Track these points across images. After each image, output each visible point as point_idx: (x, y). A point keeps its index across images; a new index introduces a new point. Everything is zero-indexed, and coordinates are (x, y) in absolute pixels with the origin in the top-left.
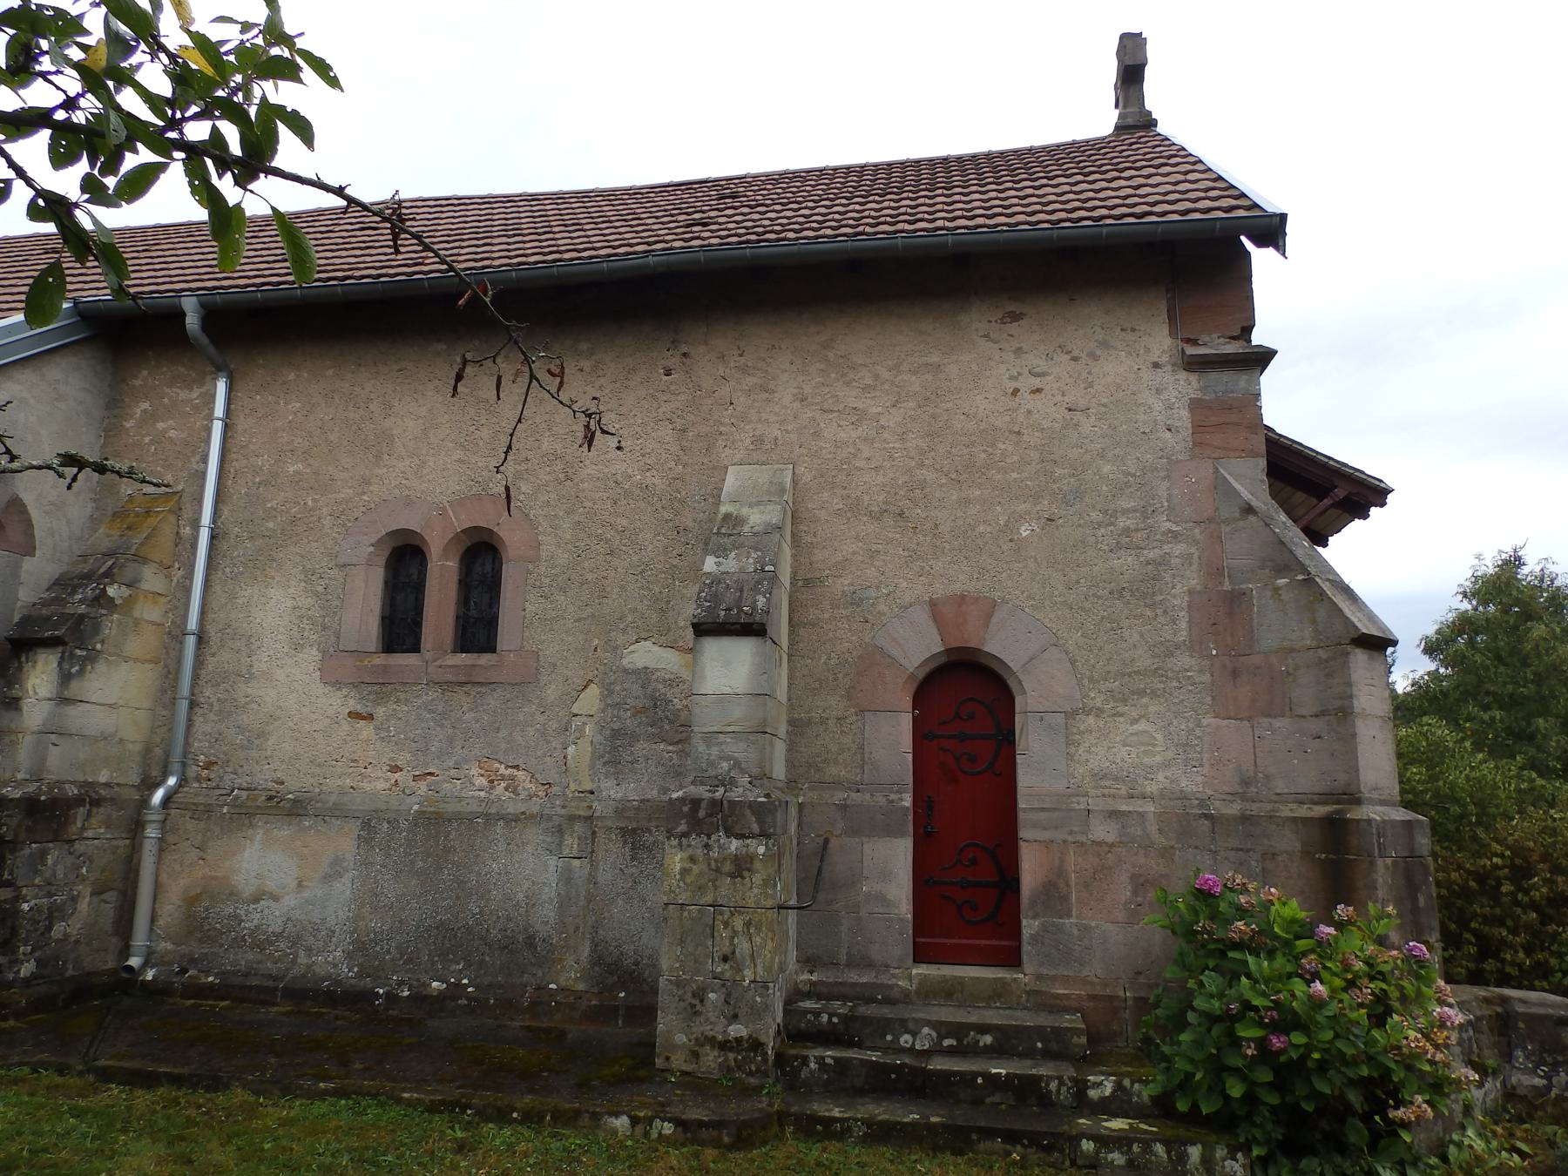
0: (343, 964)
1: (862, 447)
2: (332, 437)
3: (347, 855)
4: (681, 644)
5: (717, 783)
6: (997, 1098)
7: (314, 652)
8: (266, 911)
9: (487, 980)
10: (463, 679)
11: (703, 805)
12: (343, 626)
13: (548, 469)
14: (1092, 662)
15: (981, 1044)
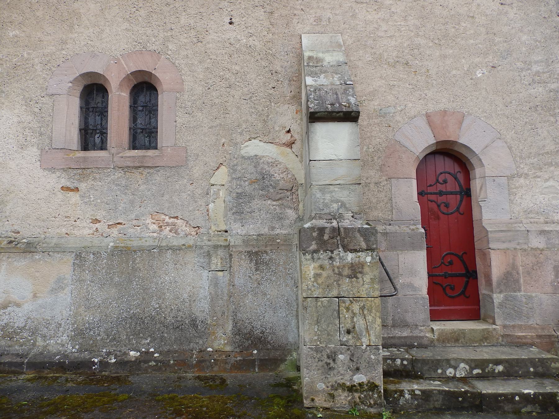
0: (68, 344)
1: (381, 24)
2: (38, 14)
3: (66, 276)
4: (277, 141)
5: (330, 217)
6: (529, 408)
7: (35, 149)
8: (12, 314)
9: (166, 348)
10: (138, 165)
11: (327, 231)
12: (54, 133)
13: (185, 35)
14: (521, 148)
15: (497, 371)
